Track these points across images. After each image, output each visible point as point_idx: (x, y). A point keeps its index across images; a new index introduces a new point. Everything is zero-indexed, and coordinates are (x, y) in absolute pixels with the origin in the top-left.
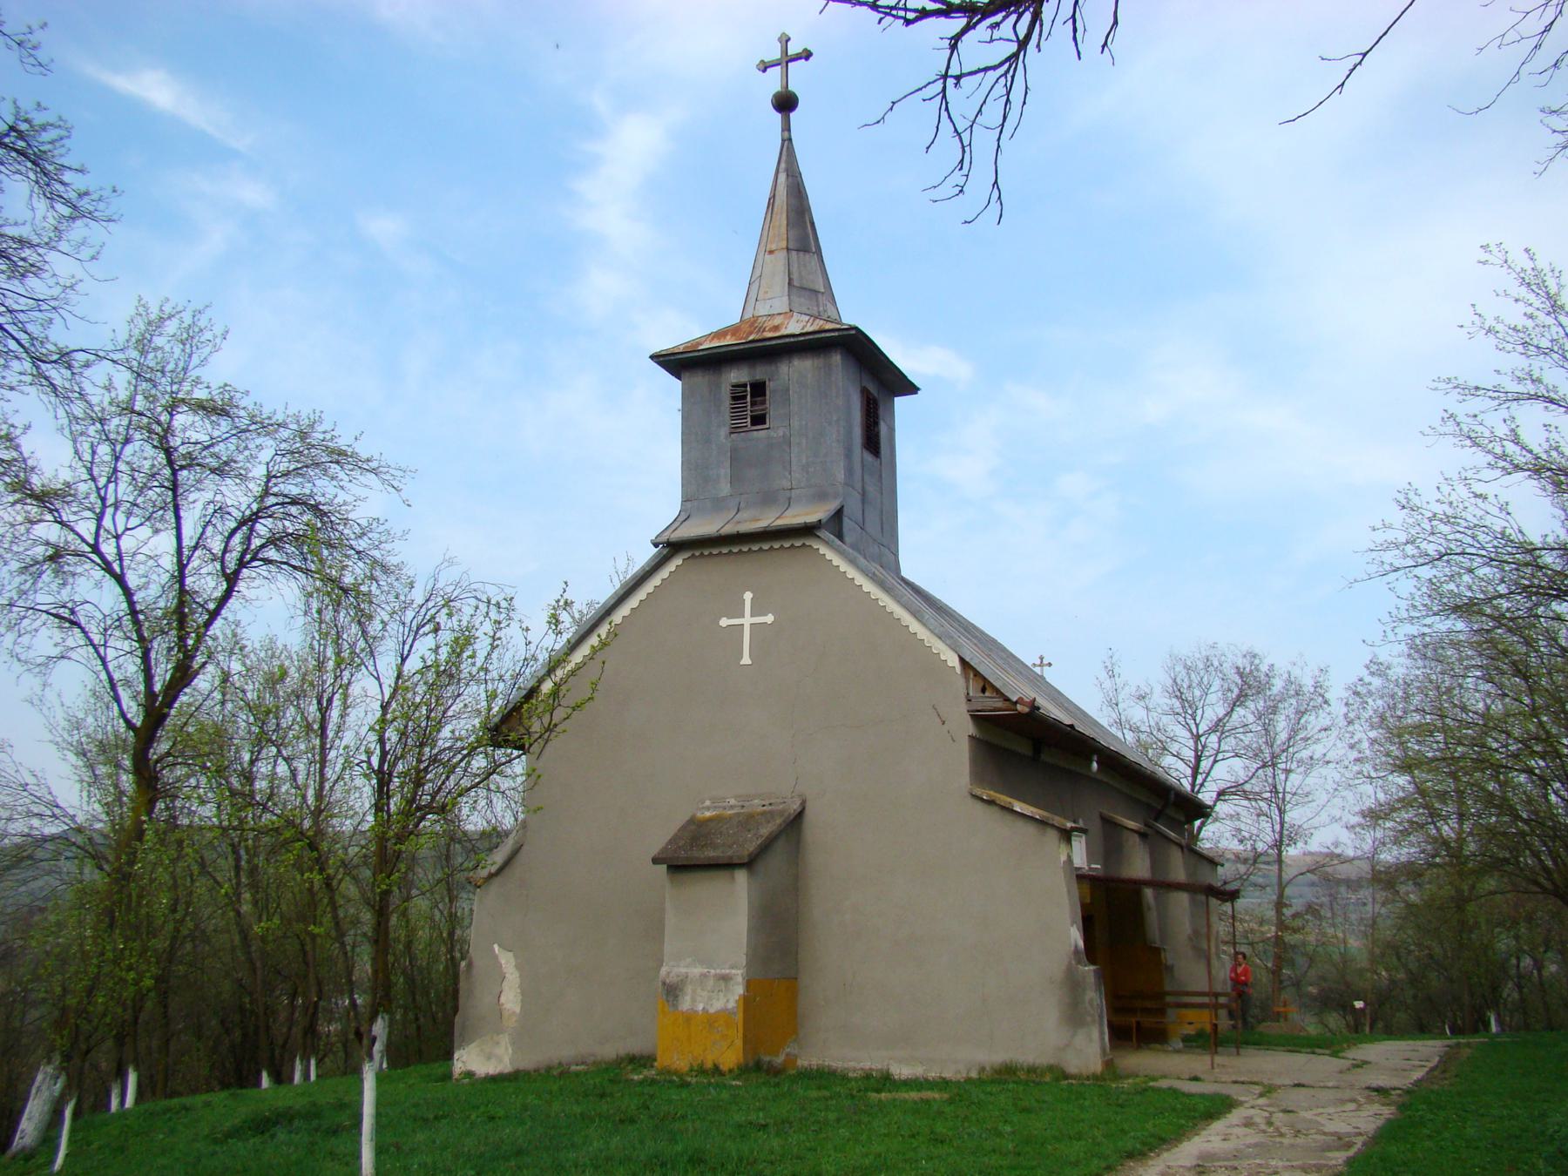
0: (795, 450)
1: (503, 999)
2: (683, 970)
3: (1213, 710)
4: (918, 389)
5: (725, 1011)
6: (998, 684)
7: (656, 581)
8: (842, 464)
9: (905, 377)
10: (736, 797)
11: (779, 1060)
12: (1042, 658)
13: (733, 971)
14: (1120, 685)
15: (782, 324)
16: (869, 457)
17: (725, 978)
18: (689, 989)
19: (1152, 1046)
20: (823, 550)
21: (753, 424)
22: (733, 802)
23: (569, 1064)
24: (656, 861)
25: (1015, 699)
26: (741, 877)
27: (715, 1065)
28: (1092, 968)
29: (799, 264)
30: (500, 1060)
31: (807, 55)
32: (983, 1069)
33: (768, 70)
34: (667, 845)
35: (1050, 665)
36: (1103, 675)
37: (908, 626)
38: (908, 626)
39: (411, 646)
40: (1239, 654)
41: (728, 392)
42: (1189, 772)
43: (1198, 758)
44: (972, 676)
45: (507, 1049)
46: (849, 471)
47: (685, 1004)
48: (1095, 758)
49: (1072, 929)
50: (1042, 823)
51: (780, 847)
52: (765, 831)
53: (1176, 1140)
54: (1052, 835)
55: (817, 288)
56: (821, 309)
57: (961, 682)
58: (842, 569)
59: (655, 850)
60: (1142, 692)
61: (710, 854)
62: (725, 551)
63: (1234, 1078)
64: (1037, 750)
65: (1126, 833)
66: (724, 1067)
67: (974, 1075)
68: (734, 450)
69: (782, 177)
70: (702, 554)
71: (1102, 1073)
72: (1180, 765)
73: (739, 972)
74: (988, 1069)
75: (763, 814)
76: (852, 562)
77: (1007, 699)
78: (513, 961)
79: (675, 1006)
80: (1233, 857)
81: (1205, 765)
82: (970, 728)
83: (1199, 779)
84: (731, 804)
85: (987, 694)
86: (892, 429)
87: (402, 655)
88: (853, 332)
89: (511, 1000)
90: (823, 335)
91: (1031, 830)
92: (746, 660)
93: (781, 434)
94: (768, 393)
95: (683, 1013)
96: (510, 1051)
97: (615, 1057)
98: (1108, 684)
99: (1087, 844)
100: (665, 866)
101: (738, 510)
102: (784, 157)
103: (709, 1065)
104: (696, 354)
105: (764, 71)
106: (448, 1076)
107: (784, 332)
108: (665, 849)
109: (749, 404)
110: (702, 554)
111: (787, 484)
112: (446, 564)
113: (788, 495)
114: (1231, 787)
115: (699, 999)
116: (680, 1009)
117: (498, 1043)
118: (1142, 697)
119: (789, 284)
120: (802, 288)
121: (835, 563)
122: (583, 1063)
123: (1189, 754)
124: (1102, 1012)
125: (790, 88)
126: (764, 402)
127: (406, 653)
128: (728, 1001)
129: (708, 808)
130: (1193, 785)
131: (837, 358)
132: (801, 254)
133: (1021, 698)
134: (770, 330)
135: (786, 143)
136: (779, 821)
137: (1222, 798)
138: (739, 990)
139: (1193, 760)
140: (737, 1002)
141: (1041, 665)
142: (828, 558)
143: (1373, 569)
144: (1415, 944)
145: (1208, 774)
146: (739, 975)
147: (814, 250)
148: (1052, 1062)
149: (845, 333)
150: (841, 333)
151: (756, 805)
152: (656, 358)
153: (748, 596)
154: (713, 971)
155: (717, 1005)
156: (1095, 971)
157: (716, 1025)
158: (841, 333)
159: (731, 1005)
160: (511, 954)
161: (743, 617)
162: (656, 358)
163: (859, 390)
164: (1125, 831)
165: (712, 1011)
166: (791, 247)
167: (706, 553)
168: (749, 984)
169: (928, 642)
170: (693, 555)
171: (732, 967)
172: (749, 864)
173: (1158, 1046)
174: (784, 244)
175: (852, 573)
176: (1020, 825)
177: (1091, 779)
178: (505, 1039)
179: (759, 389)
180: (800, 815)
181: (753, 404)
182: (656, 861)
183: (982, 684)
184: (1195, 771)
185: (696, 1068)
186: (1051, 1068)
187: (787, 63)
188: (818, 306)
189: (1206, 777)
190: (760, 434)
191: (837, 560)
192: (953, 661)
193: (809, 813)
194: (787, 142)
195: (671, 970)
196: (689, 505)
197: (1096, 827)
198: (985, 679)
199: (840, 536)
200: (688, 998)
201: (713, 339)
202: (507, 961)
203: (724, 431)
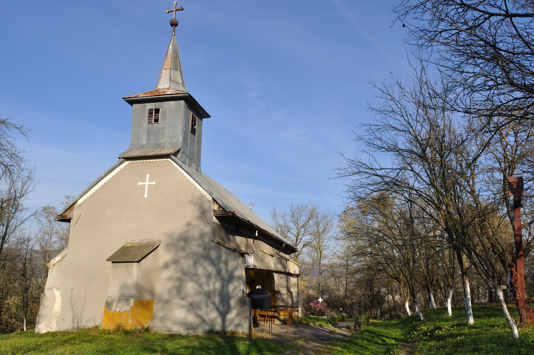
3: (302, 221)
4: (210, 116)
8: (181, 136)
15: (166, 91)
24: (108, 260)
25: (228, 211)
28: (248, 298)
29: (174, 73)
37: (197, 187)
38: (197, 187)
42: (295, 239)
45: (54, 324)
48: (257, 232)
55: (179, 82)
68: (148, 130)
77: (226, 211)
78: (59, 293)
81: (300, 237)
85: (220, 209)
88: (187, 95)
90: (178, 95)
92: (146, 196)
93: (163, 125)
96: (55, 325)
100: (111, 262)
101: (148, 149)
106: (34, 332)
107: (166, 93)
119: (170, 79)
120: (174, 81)
123: (295, 233)
125: (176, 19)
128: (127, 308)
130: (296, 242)
132: (175, 71)
134: (162, 93)
143: (337, 175)
144: (5, 322)
145: (301, 239)
147: (179, 70)
149: (185, 95)
153: (148, 176)
160: (59, 291)
161: (145, 182)
166: (171, 68)
169: (203, 192)
179: (157, 111)
181: (155, 115)
182: (108, 260)
183: (219, 206)
184: (297, 237)
188: (179, 87)
189: (300, 241)
190: (156, 125)
192: (210, 198)
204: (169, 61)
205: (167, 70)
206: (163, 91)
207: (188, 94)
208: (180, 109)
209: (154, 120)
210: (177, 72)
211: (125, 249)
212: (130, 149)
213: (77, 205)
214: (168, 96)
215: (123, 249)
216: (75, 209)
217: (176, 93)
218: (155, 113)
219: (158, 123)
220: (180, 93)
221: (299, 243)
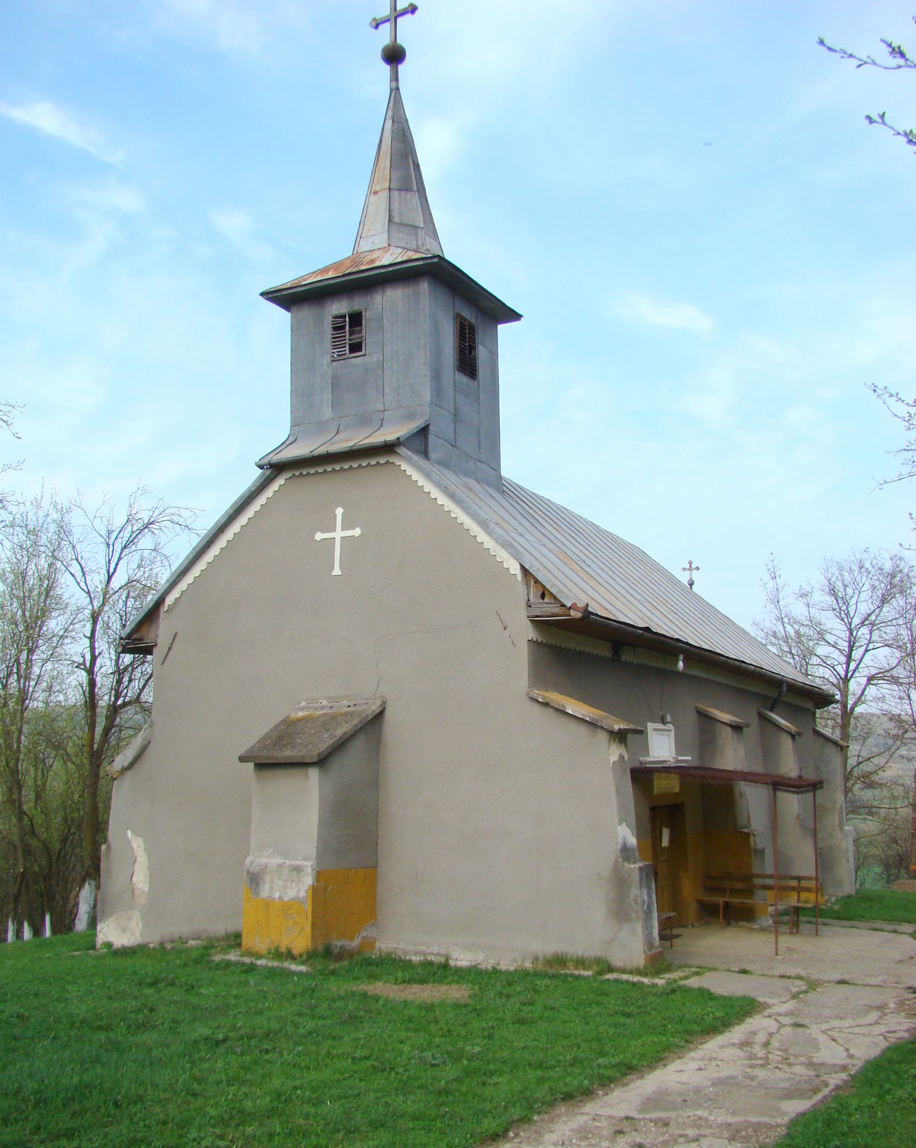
0: (387, 373)
1: (135, 879)
2: (264, 860)
3: (863, 606)
5: (295, 899)
6: (554, 591)
7: (262, 500)
8: (428, 385)
9: (504, 304)
10: (327, 698)
11: (355, 943)
12: (690, 563)
13: (305, 863)
14: (780, 585)
15: (378, 257)
16: (463, 379)
17: (297, 869)
18: (268, 878)
19: (740, 923)
20: (404, 466)
21: (351, 351)
22: (324, 702)
23: (188, 939)
24: (242, 759)
25: (569, 605)
26: (314, 774)
27: (288, 949)
29: (400, 201)
30: (133, 933)
31: (413, 9)
32: (536, 959)
33: (380, 27)
34: (256, 744)
35: (698, 568)
36: (766, 577)
39: (117, 565)
40: (888, 557)
41: (331, 326)
42: (843, 659)
43: (851, 648)
44: (532, 583)
45: (138, 923)
46: (438, 392)
47: (265, 893)
48: (681, 657)
49: (619, 828)
50: (593, 725)
51: (359, 744)
52: (340, 731)
53: (649, 1066)
54: (603, 736)
55: (417, 224)
56: (420, 243)
57: (522, 588)
58: (420, 484)
59: (243, 750)
60: (804, 591)
61: (288, 753)
62: (320, 470)
63: (782, 971)
64: (616, 651)
65: (720, 727)
66: (296, 952)
67: (528, 965)
69: (389, 124)
70: (301, 473)
71: (645, 967)
72: (836, 654)
73: (310, 863)
74: (541, 958)
75: (345, 714)
76: (428, 476)
77: (564, 606)
78: (142, 844)
79: (257, 893)
80: (883, 733)
81: (856, 654)
82: (531, 633)
83: (853, 666)
84: (322, 706)
85: (546, 600)
86: (494, 355)
87: (108, 571)
88: (436, 260)
89: (141, 880)
90: (409, 265)
91: (583, 731)
92: (337, 571)
93: (376, 360)
94: (364, 322)
95: (263, 900)
96: (141, 926)
97: (224, 933)
98: (771, 584)
99: (675, 734)
100: (252, 764)
102: (391, 105)
103: (283, 949)
104: (299, 289)
105: (377, 27)
107: (377, 264)
108: (251, 749)
109: (347, 333)
110: (301, 473)
111: (380, 406)
112: (139, 492)
113: (381, 417)
114: (880, 673)
115: (276, 887)
116: (260, 896)
117: (131, 918)
118: (805, 595)
119: (389, 221)
120: (401, 224)
121: (414, 478)
122: (199, 938)
123: (844, 645)
124: (649, 905)
126: (360, 332)
127: (112, 570)
129: (302, 709)
130: (847, 671)
131: (424, 286)
132: (403, 193)
133: (574, 604)
134: (366, 264)
135: (394, 92)
136: (355, 722)
137: (872, 682)
138: (309, 880)
139: (847, 649)
140: (306, 891)
141: (690, 569)
142: (408, 473)
145: (861, 660)
146: (309, 866)
147: (415, 188)
148: (599, 954)
149: (429, 261)
150: (425, 262)
151: (343, 707)
152: (265, 295)
153: (339, 511)
154: (288, 862)
155: (290, 894)
156: (641, 869)
157: (290, 912)
158: (425, 262)
159: (302, 894)
160: (141, 839)
162: (265, 295)
163: (451, 316)
164: (719, 725)
165: (286, 899)
167: (305, 472)
168: (319, 875)
169: (494, 551)
170: (294, 475)
171: (305, 859)
172: (322, 762)
173: (746, 924)
174: (387, 185)
175: (428, 487)
176: (573, 726)
177: (680, 674)
178: (136, 915)
179: (356, 319)
180: (379, 716)
182: (242, 759)
184: (849, 658)
185: (273, 951)
186: (598, 960)
187: (396, 18)
188: (417, 240)
189: (859, 664)
190: (357, 361)
191: (416, 476)
192: (515, 569)
193: (388, 714)
194: (395, 91)
195: (255, 860)
196: (296, 429)
197: (692, 717)
198: (544, 587)
199: (425, 454)
200: (267, 886)
201: (317, 275)
202: (138, 845)
203: (327, 360)
204: (384, 169)
205: (380, 194)
206: (369, 258)
207: (438, 256)
208: (421, 306)
209: (350, 345)
210: (409, 195)
211: (288, 726)
212: (291, 437)
213: (166, 609)
214: (382, 271)
215: (283, 727)
216: (161, 619)
217: (404, 258)
218: (350, 327)
219: (360, 354)
220: (414, 257)
221: (854, 671)
